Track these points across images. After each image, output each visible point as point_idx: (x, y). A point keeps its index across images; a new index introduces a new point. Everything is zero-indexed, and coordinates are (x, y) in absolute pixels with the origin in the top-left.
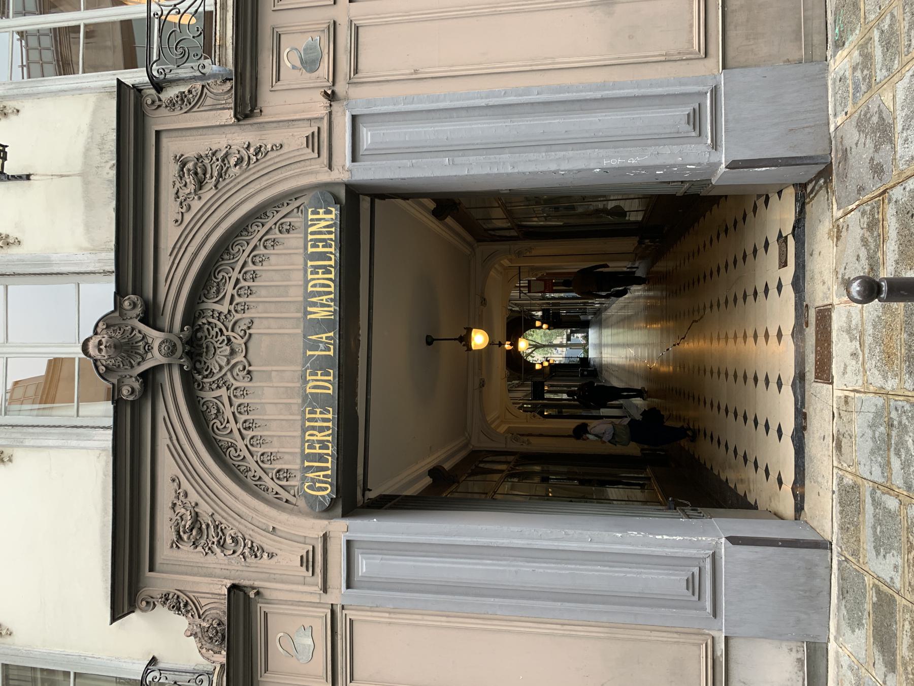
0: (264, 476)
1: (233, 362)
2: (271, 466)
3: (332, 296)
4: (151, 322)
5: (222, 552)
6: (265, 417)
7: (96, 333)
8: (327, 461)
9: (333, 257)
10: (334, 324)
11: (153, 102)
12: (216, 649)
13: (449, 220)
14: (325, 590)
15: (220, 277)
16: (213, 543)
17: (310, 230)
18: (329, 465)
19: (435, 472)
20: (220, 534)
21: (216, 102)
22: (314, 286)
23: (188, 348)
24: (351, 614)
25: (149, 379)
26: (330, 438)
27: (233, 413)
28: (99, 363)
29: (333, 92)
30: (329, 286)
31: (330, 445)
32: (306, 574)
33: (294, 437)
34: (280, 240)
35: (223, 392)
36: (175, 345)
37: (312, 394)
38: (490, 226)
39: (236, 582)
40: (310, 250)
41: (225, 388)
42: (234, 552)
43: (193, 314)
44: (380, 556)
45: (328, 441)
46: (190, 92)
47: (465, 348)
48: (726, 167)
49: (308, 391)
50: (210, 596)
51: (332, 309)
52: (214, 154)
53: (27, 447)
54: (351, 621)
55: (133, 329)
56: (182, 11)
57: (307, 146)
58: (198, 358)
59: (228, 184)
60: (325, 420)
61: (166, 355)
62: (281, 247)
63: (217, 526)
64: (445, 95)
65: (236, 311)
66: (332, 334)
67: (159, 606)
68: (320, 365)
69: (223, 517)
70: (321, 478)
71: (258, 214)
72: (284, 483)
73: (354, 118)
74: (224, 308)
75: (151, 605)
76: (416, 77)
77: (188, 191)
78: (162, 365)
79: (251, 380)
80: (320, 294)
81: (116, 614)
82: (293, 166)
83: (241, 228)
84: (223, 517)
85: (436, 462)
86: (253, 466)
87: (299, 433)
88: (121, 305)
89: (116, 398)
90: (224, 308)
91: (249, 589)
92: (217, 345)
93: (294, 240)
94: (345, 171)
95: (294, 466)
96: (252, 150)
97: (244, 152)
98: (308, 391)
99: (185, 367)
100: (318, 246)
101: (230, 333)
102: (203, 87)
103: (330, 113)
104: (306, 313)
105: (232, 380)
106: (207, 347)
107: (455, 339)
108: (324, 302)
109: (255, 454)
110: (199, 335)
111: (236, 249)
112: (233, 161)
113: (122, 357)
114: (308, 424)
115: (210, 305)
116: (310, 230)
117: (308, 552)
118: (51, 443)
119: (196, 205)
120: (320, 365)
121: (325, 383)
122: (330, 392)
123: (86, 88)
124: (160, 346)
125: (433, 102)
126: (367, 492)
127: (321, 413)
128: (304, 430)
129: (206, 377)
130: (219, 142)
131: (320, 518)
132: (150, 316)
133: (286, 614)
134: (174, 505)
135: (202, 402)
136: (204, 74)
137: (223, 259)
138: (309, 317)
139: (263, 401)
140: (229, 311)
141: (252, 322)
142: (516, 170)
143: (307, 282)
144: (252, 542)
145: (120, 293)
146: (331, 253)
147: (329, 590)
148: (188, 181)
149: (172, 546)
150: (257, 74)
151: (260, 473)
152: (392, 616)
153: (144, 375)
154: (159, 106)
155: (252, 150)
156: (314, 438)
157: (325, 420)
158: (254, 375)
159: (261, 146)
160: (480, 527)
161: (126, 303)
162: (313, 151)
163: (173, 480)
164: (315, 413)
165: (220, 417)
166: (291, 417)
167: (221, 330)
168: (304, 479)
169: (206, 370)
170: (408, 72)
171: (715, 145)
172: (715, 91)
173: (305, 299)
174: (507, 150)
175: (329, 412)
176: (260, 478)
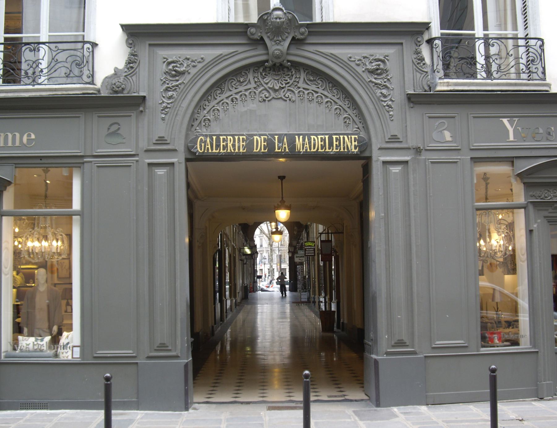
1: (270, 91)
3: (309, 150)
4: (292, 42)
8: (216, 149)
9: (331, 150)
12: (109, 87)
16: (168, 84)
17: (346, 137)
20: (174, 88)
22: (314, 140)
23: (278, 65)
24: (134, 165)
26: (229, 151)
27: (241, 92)
31: (225, 151)
35: (253, 85)
40: (334, 137)
41: (255, 86)
42: (164, 97)
43: (297, 66)
45: (227, 150)
48: (375, 359)
49: (255, 137)
51: (301, 150)
54: (130, 166)
65: (299, 92)
66: (287, 150)
68: (270, 144)
74: (301, 84)
75: (130, 45)
77: (367, 64)
80: (310, 143)
81: (126, 28)
83: (347, 95)
90: (301, 84)
92: (280, 81)
94: (378, 158)
96: (390, 103)
97: (389, 98)
98: (255, 137)
99: (267, 64)
100: (336, 142)
101: (287, 88)
102: (427, 72)
104: (299, 135)
105: (260, 90)
106: (278, 75)
110: (286, 70)
111: (335, 91)
112: (384, 91)
113: (272, 29)
114: (236, 137)
115: (303, 75)
116: (346, 137)
117: (166, 140)
119: (360, 70)
122: (255, 151)
124: (279, 50)
127: (243, 145)
129: (261, 74)
130: (394, 84)
131: (185, 147)
132: (295, 41)
134: (188, 59)
135: (247, 72)
137: (329, 83)
138: (297, 137)
140: (299, 88)
143: (316, 135)
144: (170, 108)
146: (333, 149)
148: (373, 64)
149: (164, 58)
151: (208, 109)
153: (262, 39)
154: (417, 45)
155: (390, 103)
156: (229, 142)
159: (392, 108)
164: (243, 142)
167: (288, 83)
168: (206, 136)
171: (388, 354)
172: (414, 353)
175: (244, 150)
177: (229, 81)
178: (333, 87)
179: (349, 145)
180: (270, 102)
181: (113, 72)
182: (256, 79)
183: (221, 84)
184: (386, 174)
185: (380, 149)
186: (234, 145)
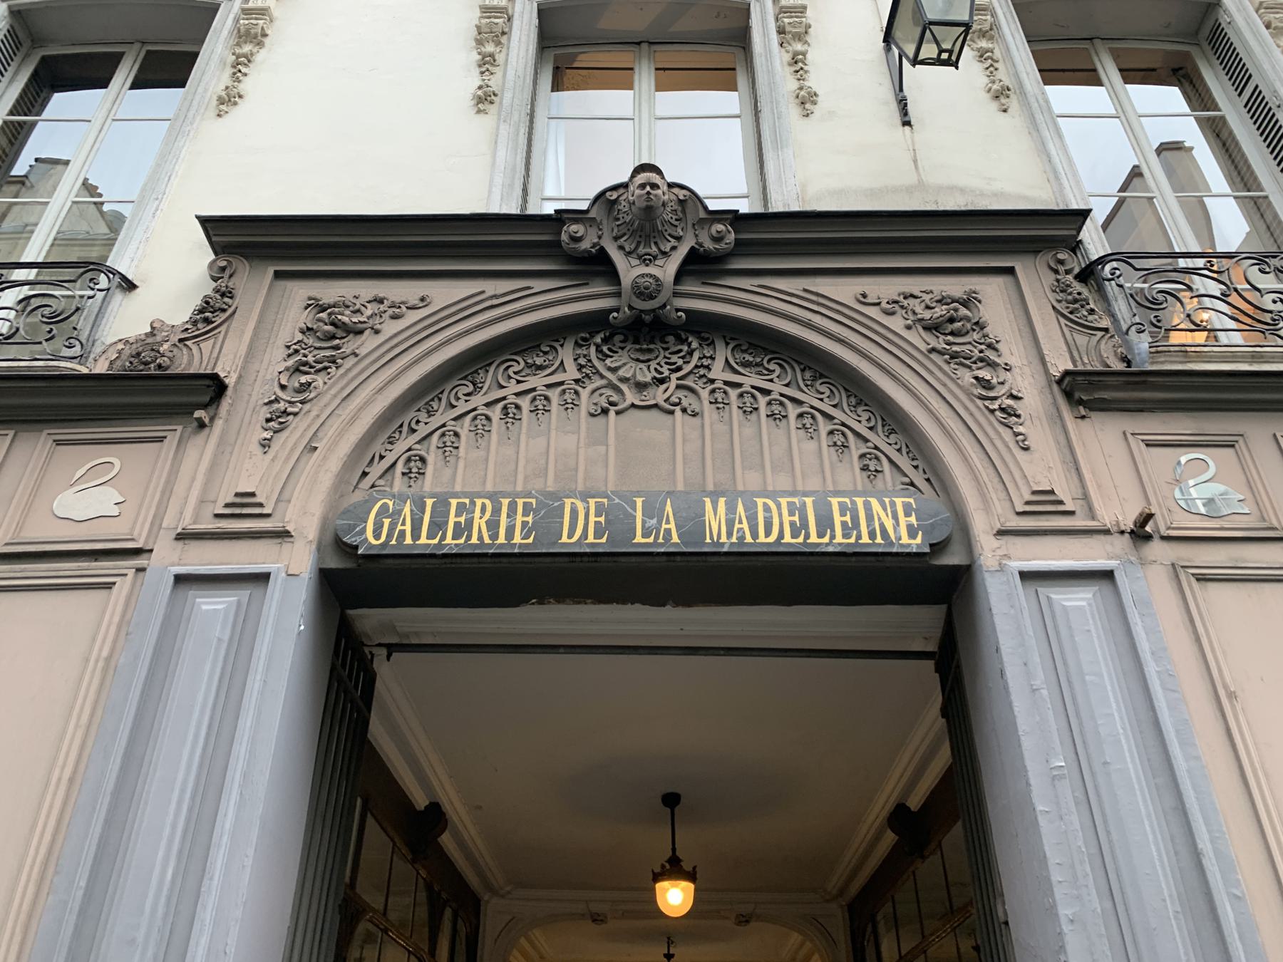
0: (417, 437)
1: (624, 387)
2: (433, 448)
3: (749, 539)
5: (287, 369)
6: (523, 437)
7: (671, 185)
10: (696, 544)
11: (1061, 262)
13: (890, 838)
14: (183, 537)
15: (772, 366)
16: (305, 356)
17: (874, 502)
18: (423, 540)
19: (435, 816)
20: (320, 366)
21: (1083, 350)
22: (767, 509)
24: (123, 587)
25: (597, 265)
26: (474, 540)
27: (534, 390)
28: (621, 191)
29: (1148, 537)
30: (768, 534)
32: (221, 502)
33: (484, 482)
34: (846, 457)
35: (572, 373)
36: (652, 297)
37: (562, 507)
38: (882, 928)
39: (229, 392)
40: (835, 501)
41: (578, 376)
42: (283, 387)
43: (707, 328)
44: (226, 638)
45: (469, 537)
46: (1092, 311)
47: (658, 870)
49: (568, 502)
50: (215, 355)
51: (724, 539)
52: (990, 346)
53: (498, 128)
54: (109, 586)
55: (678, 239)
56: (1229, 299)
57: (1034, 493)
58: (631, 338)
59: (940, 369)
60: (510, 531)
61: (635, 286)
62: (835, 457)
63: (334, 362)
64: (1198, 758)
65: (713, 391)
66: (675, 539)
67: (214, 284)
68: (617, 519)
69: (349, 370)
70: (399, 527)
71: (891, 418)
72: (400, 467)
73: (1108, 575)
74: (718, 372)
76: (1221, 700)
78: (620, 284)
79: (592, 415)
82: (991, 471)
83: (861, 392)
84: (349, 370)
85: (455, 818)
86: (436, 421)
87: (489, 487)
88: (719, 221)
89: (566, 216)
91: (212, 414)
92: (653, 365)
93: (849, 473)
94: (999, 562)
95: (428, 483)
96: (1010, 402)
98: (568, 502)
99: (615, 314)
100: (843, 514)
102: (1106, 330)
103: (1107, 532)
105: (590, 387)
106: (650, 351)
107: (674, 849)
108: (737, 526)
109: (459, 423)
110: (671, 339)
111: (822, 389)
112: (985, 374)
113: (631, 223)
114: (505, 502)
115: (722, 353)
116: (874, 502)
117: (261, 505)
118: (502, 153)
119: (896, 323)
120: (617, 519)
121: (581, 529)
122: (565, 539)
123: (1061, 184)
124: (651, 276)
125: (1177, 731)
126: (384, 652)
127: (524, 524)
128: (494, 497)
129: (599, 350)
130: (1013, 351)
132: (700, 265)
133: (153, 472)
134: (381, 301)
135: (556, 345)
136: (1127, 333)
137: (803, 371)
138: (707, 500)
139: (553, 433)
140: (712, 381)
141: (695, 415)
142: (1066, 928)
143: (773, 495)
144: (295, 414)
145: (734, 218)
147: (180, 543)
150: (1151, 410)
151: (423, 430)
152: (101, 664)
154: (1056, 272)
157: (510, 531)
158: (601, 420)
159: (1018, 416)
160: (251, 852)
161: (720, 227)
162: (1028, 503)
163: (422, 299)
165: (528, 371)
166: (520, 477)
167: (679, 369)
169: (610, 350)
170: (1228, 679)
173: (742, 494)
174: (1108, 905)
176: (414, 431)
177: (498, 366)
178: (814, 379)
179: (889, 524)
180: (621, 416)
181: (149, 330)
182: (582, 361)
183: (476, 372)
184: (1046, 620)
185: (1001, 533)
186: (493, 525)
